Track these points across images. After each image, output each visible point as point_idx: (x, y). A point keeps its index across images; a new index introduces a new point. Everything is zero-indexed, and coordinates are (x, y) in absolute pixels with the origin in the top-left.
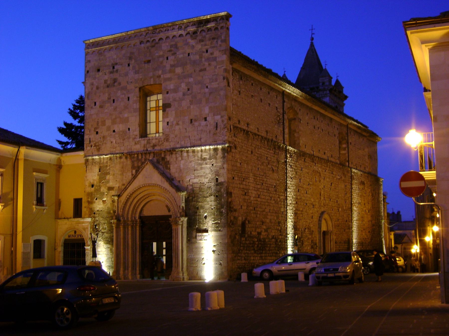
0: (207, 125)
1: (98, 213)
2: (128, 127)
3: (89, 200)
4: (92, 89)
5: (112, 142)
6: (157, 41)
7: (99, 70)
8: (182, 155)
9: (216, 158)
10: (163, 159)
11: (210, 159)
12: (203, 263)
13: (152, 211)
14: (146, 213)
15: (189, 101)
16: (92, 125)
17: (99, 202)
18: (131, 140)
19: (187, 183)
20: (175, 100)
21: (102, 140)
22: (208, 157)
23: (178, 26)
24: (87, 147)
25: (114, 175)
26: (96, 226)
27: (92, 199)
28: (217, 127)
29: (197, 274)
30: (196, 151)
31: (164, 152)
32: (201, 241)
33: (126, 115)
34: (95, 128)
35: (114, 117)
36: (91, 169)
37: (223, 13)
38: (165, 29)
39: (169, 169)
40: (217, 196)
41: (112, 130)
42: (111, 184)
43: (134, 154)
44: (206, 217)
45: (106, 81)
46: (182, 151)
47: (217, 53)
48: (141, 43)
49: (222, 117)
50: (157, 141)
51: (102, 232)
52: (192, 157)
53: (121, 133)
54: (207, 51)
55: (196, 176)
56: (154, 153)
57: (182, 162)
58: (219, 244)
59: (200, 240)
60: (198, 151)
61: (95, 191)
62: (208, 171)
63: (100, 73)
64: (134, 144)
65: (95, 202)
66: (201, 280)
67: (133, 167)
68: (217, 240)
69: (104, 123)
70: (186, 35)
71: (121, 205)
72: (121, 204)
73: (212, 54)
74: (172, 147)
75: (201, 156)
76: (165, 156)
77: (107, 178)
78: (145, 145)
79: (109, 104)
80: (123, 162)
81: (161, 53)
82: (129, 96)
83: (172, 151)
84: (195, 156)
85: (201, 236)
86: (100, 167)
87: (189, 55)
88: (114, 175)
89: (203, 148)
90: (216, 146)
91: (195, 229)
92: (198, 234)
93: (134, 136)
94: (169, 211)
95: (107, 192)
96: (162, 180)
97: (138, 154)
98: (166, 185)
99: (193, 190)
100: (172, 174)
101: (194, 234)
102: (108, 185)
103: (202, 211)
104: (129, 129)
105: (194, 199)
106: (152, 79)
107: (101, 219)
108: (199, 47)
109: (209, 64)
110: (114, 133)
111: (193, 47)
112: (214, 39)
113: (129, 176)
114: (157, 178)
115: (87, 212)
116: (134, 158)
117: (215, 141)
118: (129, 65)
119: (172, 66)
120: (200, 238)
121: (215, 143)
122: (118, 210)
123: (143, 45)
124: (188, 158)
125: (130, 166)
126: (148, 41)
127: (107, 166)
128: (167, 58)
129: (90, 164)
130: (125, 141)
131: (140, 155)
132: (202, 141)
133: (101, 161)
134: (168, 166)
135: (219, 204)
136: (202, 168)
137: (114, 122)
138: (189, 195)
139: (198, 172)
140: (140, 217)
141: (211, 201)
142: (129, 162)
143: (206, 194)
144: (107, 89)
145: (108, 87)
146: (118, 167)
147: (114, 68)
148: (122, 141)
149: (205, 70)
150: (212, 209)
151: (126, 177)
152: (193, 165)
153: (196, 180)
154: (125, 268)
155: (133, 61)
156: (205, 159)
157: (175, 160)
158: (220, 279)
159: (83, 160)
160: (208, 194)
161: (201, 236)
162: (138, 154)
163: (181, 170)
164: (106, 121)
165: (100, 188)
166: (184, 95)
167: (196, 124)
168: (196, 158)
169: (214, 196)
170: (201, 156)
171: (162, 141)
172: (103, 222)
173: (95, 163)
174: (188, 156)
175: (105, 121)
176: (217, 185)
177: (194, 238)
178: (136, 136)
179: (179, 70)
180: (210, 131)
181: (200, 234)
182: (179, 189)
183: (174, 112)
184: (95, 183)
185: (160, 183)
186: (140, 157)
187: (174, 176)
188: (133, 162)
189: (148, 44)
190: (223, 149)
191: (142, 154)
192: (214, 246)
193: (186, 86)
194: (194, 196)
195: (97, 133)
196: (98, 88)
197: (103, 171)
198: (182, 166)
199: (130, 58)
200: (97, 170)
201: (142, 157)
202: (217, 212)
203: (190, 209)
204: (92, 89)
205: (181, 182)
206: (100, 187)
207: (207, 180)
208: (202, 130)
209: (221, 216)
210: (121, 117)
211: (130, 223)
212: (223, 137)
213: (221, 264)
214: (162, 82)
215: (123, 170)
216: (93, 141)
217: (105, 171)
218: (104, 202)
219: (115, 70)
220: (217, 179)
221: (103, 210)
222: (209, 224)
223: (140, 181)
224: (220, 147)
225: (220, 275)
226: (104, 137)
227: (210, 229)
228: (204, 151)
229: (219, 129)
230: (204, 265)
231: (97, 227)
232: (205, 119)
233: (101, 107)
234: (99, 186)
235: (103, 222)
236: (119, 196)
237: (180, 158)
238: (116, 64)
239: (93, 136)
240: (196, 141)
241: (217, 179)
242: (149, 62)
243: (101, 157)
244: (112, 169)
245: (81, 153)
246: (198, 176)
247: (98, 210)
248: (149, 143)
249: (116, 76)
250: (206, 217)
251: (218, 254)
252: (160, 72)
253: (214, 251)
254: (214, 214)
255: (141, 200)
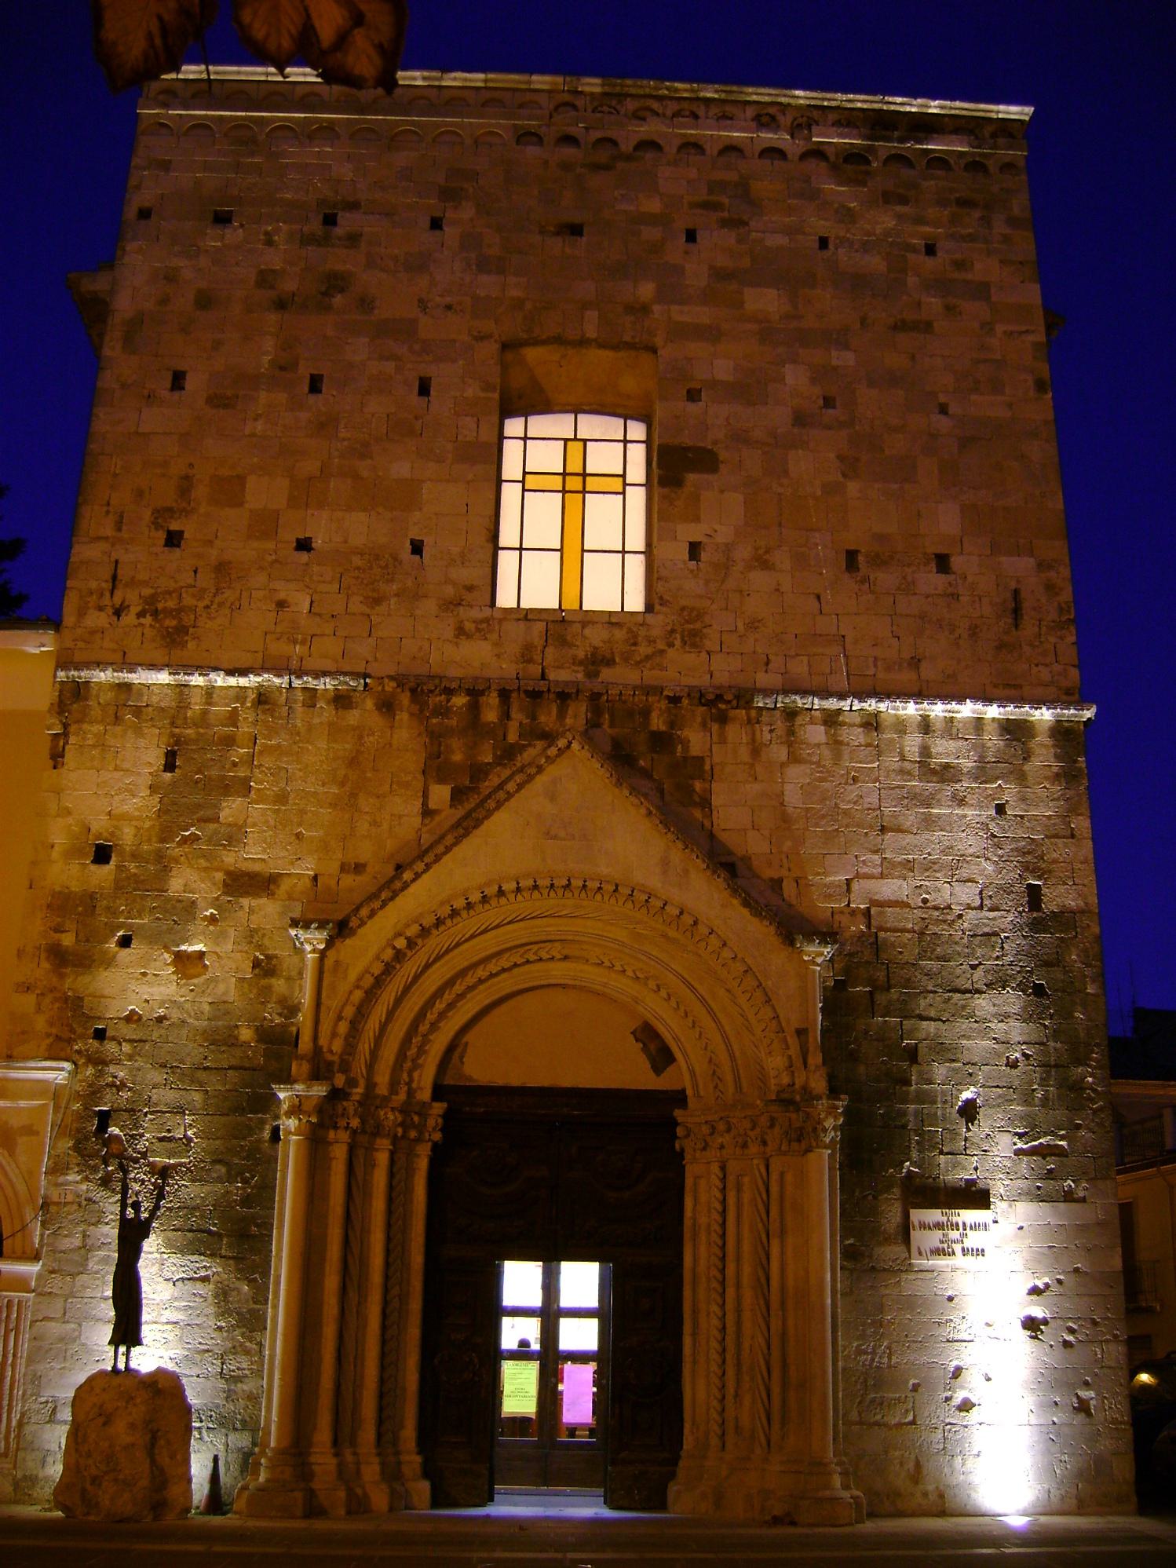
0: (955, 596)
1: (129, 1031)
2: (415, 533)
3: (68, 940)
4: (165, 301)
5: (281, 604)
6: (627, 146)
7: (222, 219)
8: (791, 732)
9: (1021, 778)
10: (662, 742)
11: (982, 774)
12: (959, 1397)
13: (515, 1055)
14: (484, 1067)
15: (832, 455)
16: (140, 494)
17: (145, 961)
18: (430, 606)
19: (828, 897)
20: (740, 438)
21: (206, 580)
22: (967, 764)
23: (750, 112)
24: (82, 613)
25: (282, 798)
26: (104, 1119)
27: (91, 937)
28: (1017, 612)
29: (917, 1474)
31: (675, 700)
32: (941, 1262)
33: (401, 469)
34: (162, 514)
35: (310, 467)
36: (103, 746)
37: (1013, 109)
38: (672, 107)
39: (705, 803)
40: (1039, 991)
41: (290, 537)
42: (253, 854)
43: (449, 692)
44: (969, 1111)
45: (265, 278)
46: (791, 714)
47: (985, 268)
48: (526, 137)
49: (1042, 566)
50: (619, 634)
51: (153, 1169)
52: (865, 752)
53: (357, 561)
54: (930, 250)
55: (893, 865)
56: (595, 697)
57: (797, 777)
58: (1070, 1281)
59: (938, 1252)
60: (901, 726)
61: (118, 886)
62: (971, 843)
63: (233, 234)
64: (449, 633)
65: (109, 962)
66: (943, 1513)
67: (436, 767)
68: (1053, 1254)
69: (230, 491)
70: (804, 156)
71: (344, 993)
72: (343, 987)
73: (960, 265)
74: (722, 679)
75: (925, 751)
76: (672, 724)
78: (528, 648)
79: (282, 397)
80: (359, 732)
81: (654, 206)
82: (431, 371)
85: (939, 1226)
86: (178, 740)
87: (823, 243)
88: (282, 798)
89: (938, 710)
90: (1011, 711)
91: (895, 1182)
92: (918, 1215)
93: (449, 591)
95: (215, 903)
96: (665, 863)
98: (704, 894)
100: (723, 837)
101: (892, 1215)
102: (229, 859)
103: (940, 1071)
104: (417, 548)
105: (881, 999)
106: (592, 315)
107: (158, 1076)
108: (885, 221)
109: (949, 308)
110: (304, 557)
111: (847, 216)
112: (963, 203)
113: (399, 816)
114: (628, 841)
115: (40, 1023)
116: (444, 711)
117: (1008, 686)
118: (436, 224)
119: (720, 275)
120: (934, 1238)
121: (1012, 692)
123: (532, 151)
124: (837, 757)
125: (412, 761)
126: (569, 140)
127: (229, 741)
128: (691, 236)
129: (96, 712)
130: (381, 609)
131: (493, 699)
132: (927, 671)
133: (182, 705)
134: (698, 785)
135: (1056, 1034)
136: (929, 823)
137: (305, 494)
138: (847, 971)
140: (439, 1091)
141: (1003, 1018)
142: (405, 733)
143: (959, 969)
144: (273, 317)
145: (281, 305)
146: (320, 751)
147: (330, 220)
148: (357, 605)
149: (927, 327)
150: (1013, 1065)
151: (375, 823)
153: (892, 888)
155: (467, 212)
156: (946, 773)
157: (744, 754)
158: (1081, 1507)
159: (40, 694)
160: (979, 974)
161: (939, 1226)
163: (786, 819)
164: (251, 482)
165: (166, 869)
166: (801, 419)
167: (886, 579)
168: (892, 760)
169: (1022, 987)
170: (925, 751)
171: (651, 641)
172: (167, 1096)
173: (138, 711)
174: (836, 744)
175: (242, 480)
176: (1037, 926)
177: (888, 1240)
178: (470, 589)
179: (765, 301)
180: (974, 631)
181: (935, 1215)
183: (736, 499)
184: (128, 836)
186: (491, 715)
188: (436, 739)
189: (569, 152)
190: (1061, 732)
191: (504, 695)
192: (1035, 1291)
193: (813, 381)
194: (881, 975)
195: (173, 540)
196: (205, 301)
197: (196, 764)
198: (793, 798)
199: (449, 195)
200: (154, 757)
201: (506, 715)
202: (1043, 1082)
204: (165, 301)
205: (789, 889)
206: (164, 865)
207: (967, 894)
208: (922, 616)
209: (1076, 1108)
210: (365, 474)
212: (1057, 668)
213: (1083, 1407)
214: (658, 341)
215: (356, 776)
216: (133, 583)
218: (187, 964)
219: (339, 231)
220: (1034, 893)
221: (175, 1015)
222: (995, 1151)
224: (1044, 715)
225: (1084, 1484)
226: (222, 569)
227: (999, 1187)
228: (939, 726)
229: (1029, 628)
230: (974, 1416)
231: (114, 1130)
232: (942, 563)
233: (218, 401)
234: (159, 856)
235: (167, 1096)
237: (781, 753)
238: (354, 206)
239: (142, 555)
240: (888, 669)
241: (1034, 893)
242: (576, 230)
243: (197, 680)
244: (268, 762)
245: (38, 645)
246: (909, 865)
247: (132, 1018)
248: (563, 642)
249: (339, 260)
250: (969, 1111)
251: (1067, 1344)
252: (646, 290)
253: (1031, 1325)
254: (1027, 1098)
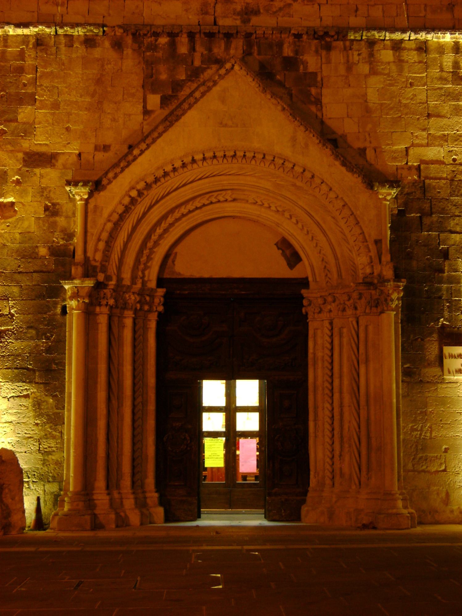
8: (371, 55)
10: (291, 63)
14: (186, 267)
19: (395, 159)
25: (56, 106)
30: (432, 47)
31: (298, 36)
39: (318, 102)
42: (40, 141)
43: (156, 35)
46: (372, 43)
52: (418, 66)
55: (435, 138)
56: (248, 36)
57: (375, 82)
67: (150, 84)
71: (101, 224)
72: (101, 221)
74: (328, 21)
76: (297, 52)
77: (20, 117)
83: (327, 38)
84: (427, 66)
88: (56, 106)
92: (448, 350)
94: (294, 258)
96: (294, 139)
97: (173, 36)
98: (318, 159)
99: (423, 187)
100: (328, 122)
101: (432, 349)
102: (26, 145)
105: (427, 221)
116: (153, 47)
122: (85, 242)
127: (21, 70)
131: (184, 39)
134: (313, 91)
138: (406, 204)
139: (445, 121)
140: (161, 282)
151: (114, 120)
152: (422, 97)
154: (112, 484)
157: (342, 70)
162: (173, 36)
163: (368, 110)
168: (435, 72)
174: (400, 62)
177: (429, 365)
182: (373, 178)
185: (283, 148)
186: (183, 49)
187: (340, 132)
188: (150, 65)
191: (191, 36)
194: (427, 206)
198: (373, 97)
201: (193, 49)
203: (410, 256)
205: (370, 154)
211: (132, 298)
215: (101, 90)
217: (12, 90)
223: (193, 132)
236: (97, 186)
237: (365, 69)
243: (60, 31)
244: (46, 83)
255: (177, 215)
